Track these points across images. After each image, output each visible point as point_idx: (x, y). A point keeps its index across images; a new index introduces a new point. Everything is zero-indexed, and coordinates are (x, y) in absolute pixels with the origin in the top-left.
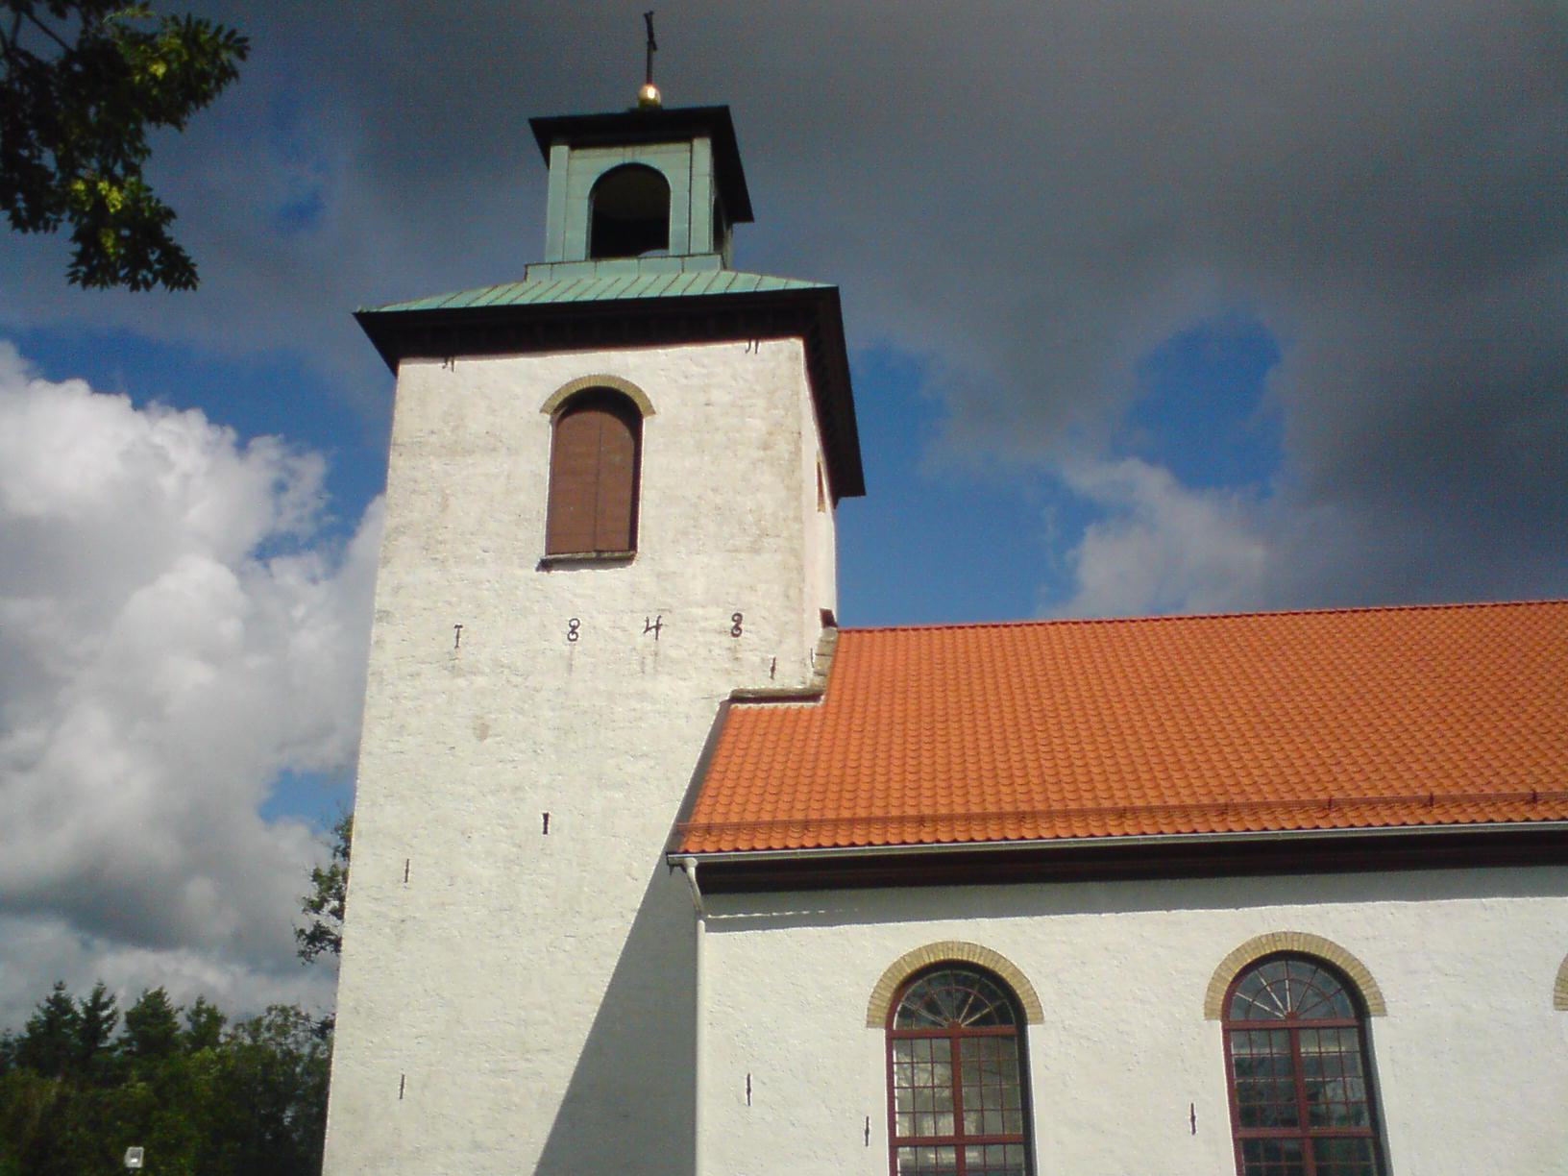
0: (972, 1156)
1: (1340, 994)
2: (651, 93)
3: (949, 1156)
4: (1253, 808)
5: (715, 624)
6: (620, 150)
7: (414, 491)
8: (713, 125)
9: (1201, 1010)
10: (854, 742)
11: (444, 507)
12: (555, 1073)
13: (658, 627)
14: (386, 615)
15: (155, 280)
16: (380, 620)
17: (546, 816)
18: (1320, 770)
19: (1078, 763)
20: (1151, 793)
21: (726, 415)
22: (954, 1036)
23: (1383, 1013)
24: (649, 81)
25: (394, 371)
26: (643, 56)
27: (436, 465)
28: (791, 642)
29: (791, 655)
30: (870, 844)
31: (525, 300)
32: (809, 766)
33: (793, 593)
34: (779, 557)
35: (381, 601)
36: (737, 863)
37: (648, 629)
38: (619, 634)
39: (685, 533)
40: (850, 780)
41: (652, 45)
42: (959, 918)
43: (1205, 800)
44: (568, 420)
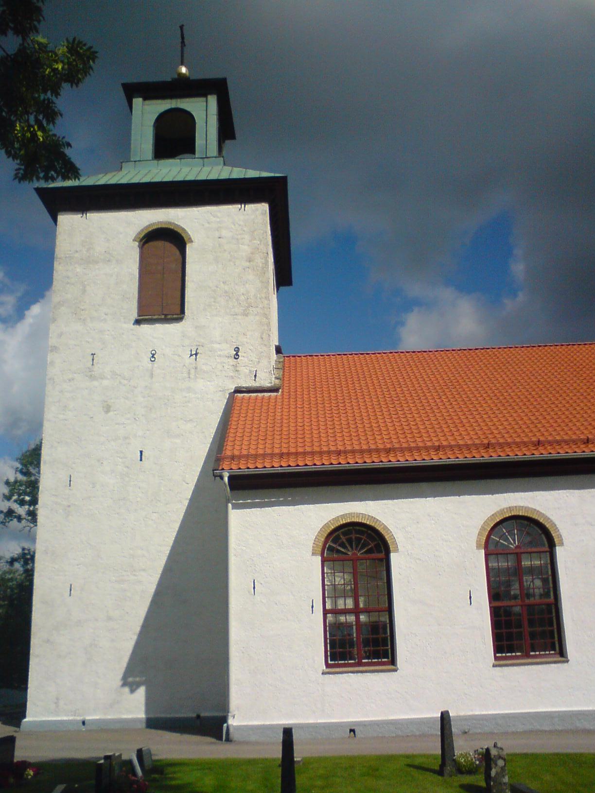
0: (362, 618)
1: (537, 534)
2: (184, 70)
3: (351, 618)
4: (501, 445)
5: (226, 353)
6: (169, 101)
7: (68, 283)
8: (217, 87)
9: (475, 544)
10: (299, 413)
11: (84, 291)
12: (148, 581)
13: (196, 354)
14: (55, 349)
15: (58, 177)
16: (52, 351)
17: (141, 452)
18: (531, 426)
19: (412, 423)
20: (450, 438)
21: (228, 242)
22: (355, 560)
23: (562, 544)
24: (182, 64)
25: (55, 220)
26: (180, 48)
27: (79, 270)
28: (264, 362)
29: (262, 369)
30: (315, 465)
31: (124, 181)
32: (279, 425)
33: (264, 336)
34: (257, 318)
35: (53, 341)
36: (305, 472)
37: (191, 355)
38: (176, 358)
39: (210, 305)
40: (300, 432)
41: (183, 42)
42: (539, 490)
43: (477, 442)
44: (147, 245)
